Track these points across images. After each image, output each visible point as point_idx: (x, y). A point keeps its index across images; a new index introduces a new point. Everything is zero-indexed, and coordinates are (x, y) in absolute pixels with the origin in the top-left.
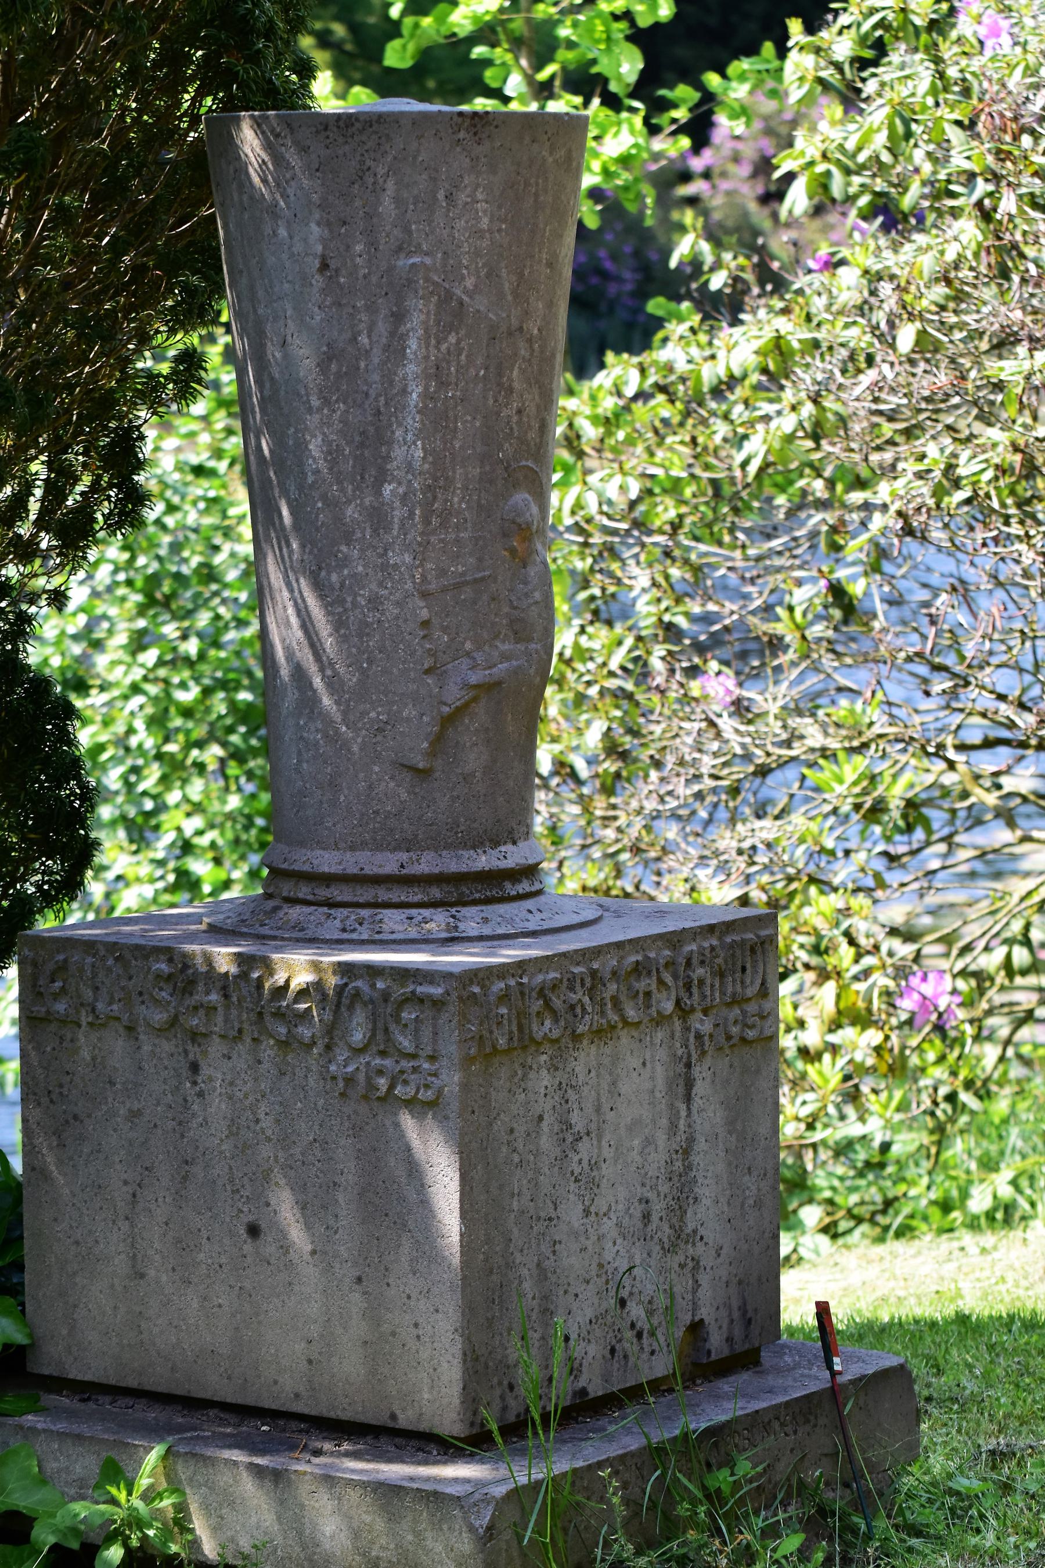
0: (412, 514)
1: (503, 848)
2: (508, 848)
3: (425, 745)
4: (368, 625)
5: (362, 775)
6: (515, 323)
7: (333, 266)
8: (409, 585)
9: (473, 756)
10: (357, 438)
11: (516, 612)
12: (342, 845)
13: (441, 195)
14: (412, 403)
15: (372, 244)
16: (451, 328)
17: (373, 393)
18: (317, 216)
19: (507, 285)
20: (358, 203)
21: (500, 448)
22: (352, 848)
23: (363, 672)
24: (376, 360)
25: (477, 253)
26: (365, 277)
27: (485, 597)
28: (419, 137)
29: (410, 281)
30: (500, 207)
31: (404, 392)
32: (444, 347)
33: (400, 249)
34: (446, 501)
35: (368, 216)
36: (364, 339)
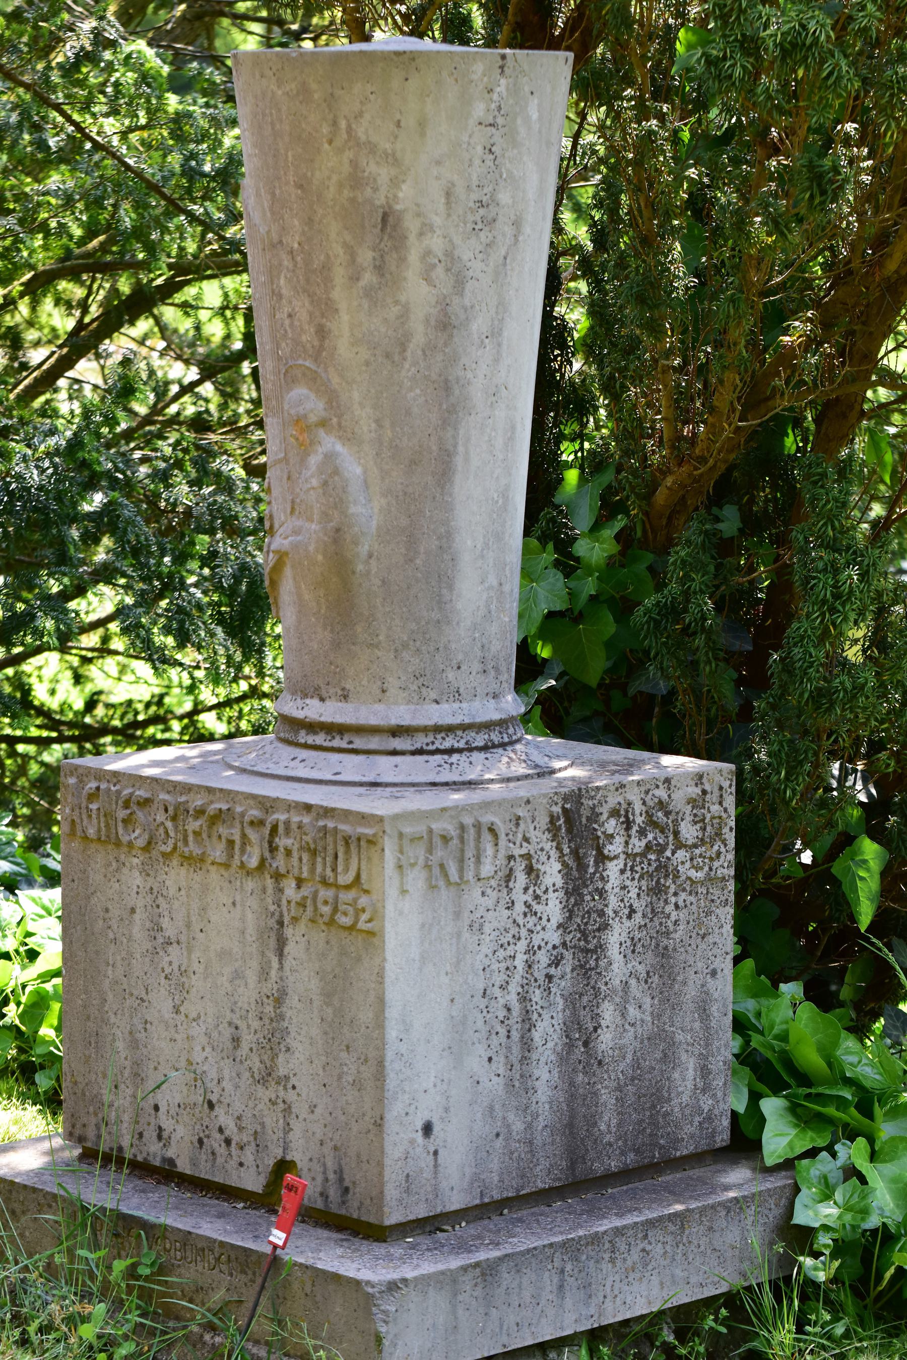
1: (308, 701)
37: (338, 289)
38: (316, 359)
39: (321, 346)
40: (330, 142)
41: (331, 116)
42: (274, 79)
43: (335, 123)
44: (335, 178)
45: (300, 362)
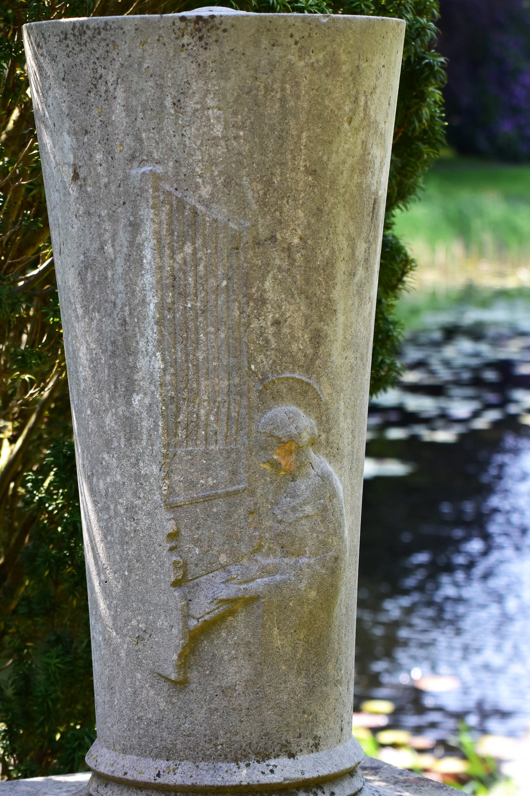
0: (156, 425)
1: (272, 762)
2: (283, 761)
3: (175, 657)
4: (127, 533)
5: (128, 681)
6: (263, 233)
7: (81, 176)
8: (157, 497)
9: (232, 670)
10: (110, 348)
11: (281, 527)
12: (118, 747)
13: (168, 102)
14: (151, 314)
15: (109, 153)
16: (183, 239)
17: (119, 302)
18: (67, 125)
19: (250, 194)
20: (95, 112)
21: (251, 359)
22: (124, 751)
23: (126, 579)
24: (120, 270)
25: (212, 162)
26: (106, 186)
27: (241, 511)
28: (143, 43)
29: (142, 189)
30: (235, 113)
31: (144, 302)
32: (179, 257)
33: (133, 157)
34: (191, 413)
35: (104, 125)
36: (109, 249)
37: (338, 287)
38: (308, 369)
40: (350, 123)
41: (353, 92)
42: (294, 49)
43: (356, 101)
44: (349, 161)
45: (287, 375)
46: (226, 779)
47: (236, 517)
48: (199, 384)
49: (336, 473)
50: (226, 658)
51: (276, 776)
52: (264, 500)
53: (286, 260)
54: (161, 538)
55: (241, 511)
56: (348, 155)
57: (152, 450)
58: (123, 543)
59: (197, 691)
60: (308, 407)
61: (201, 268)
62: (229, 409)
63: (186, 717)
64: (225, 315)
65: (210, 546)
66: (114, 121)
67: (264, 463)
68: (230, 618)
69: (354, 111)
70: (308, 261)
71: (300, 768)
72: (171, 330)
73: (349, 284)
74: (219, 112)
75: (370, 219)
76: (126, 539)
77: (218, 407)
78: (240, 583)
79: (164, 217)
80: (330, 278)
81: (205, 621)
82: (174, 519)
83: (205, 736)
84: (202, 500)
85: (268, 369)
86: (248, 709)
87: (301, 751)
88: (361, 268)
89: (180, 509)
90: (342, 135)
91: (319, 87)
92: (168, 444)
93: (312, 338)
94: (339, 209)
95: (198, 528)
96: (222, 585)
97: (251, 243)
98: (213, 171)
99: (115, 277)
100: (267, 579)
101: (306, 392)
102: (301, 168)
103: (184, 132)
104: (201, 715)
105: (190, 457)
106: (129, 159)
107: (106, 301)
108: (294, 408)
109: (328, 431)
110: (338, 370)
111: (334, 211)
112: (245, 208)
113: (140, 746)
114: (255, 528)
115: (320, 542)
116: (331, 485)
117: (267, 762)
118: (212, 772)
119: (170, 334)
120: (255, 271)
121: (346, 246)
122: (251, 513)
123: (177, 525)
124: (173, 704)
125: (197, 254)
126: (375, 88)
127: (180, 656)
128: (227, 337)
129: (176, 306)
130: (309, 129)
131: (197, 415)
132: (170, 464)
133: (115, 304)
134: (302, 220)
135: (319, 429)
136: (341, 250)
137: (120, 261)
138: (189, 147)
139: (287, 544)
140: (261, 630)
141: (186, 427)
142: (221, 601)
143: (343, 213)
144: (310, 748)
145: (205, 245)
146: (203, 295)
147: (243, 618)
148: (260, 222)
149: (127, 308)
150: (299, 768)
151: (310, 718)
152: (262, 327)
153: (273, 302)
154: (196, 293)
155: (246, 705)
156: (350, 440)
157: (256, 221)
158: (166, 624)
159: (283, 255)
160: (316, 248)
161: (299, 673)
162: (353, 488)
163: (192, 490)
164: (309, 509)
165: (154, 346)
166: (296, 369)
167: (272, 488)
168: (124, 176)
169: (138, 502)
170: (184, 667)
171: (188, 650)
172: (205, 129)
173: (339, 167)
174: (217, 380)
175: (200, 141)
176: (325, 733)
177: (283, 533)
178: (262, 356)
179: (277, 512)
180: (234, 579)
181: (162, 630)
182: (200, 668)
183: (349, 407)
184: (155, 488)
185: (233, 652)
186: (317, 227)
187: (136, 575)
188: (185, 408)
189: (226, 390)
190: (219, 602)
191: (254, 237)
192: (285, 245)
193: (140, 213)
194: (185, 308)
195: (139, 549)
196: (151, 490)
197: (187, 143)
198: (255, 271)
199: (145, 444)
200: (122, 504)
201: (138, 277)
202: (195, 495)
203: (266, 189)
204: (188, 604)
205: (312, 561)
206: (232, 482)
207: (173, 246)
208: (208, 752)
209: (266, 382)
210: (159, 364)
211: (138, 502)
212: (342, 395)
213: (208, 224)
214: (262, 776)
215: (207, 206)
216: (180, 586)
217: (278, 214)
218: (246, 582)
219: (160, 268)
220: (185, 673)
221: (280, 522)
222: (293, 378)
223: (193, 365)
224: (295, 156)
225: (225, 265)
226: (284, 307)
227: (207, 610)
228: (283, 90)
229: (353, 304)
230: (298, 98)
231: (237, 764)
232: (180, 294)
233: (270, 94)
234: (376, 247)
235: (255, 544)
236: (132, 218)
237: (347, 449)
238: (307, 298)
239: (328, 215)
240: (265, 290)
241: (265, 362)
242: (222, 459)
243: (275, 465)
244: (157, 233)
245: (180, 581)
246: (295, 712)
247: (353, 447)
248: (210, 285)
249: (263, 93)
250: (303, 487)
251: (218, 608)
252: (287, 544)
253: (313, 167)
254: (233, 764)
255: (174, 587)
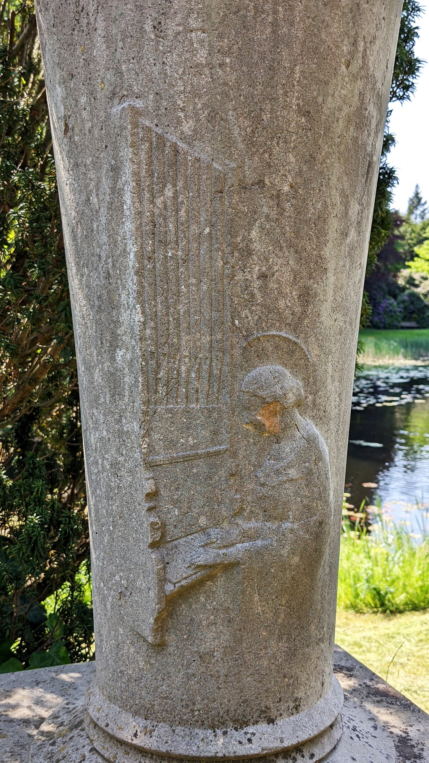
0: (137, 381)
1: (251, 729)
2: (263, 727)
3: (152, 620)
6: (251, 176)
8: (137, 455)
10: (97, 303)
11: (264, 490)
13: (148, 28)
14: (131, 264)
15: (92, 94)
17: (103, 255)
20: (78, 52)
24: (103, 220)
25: (196, 93)
27: (223, 473)
30: (221, 36)
32: (159, 201)
34: (171, 369)
36: (94, 200)
37: (330, 245)
38: (295, 328)
39: (304, 312)
40: (348, 66)
43: (355, 44)
44: (346, 110)
46: (201, 748)
47: (217, 478)
48: (179, 339)
49: (322, 436)
50: (204, 623)
51: (253, 747)
52: (247, 462)
53: (275, 209)
54: (140, 497)
55: (223, 473)
56: (344, 102)
57: (133, 406)
58: (110, 498)
59: (175, 655)
60: (295, 368)
61: (182, 213)
62: (211, 366)
63: (163, 680)
64: (208, 265)
65: (189, 508)
66: (95, 57)
67: (247, 423)
68: (209, 583)
69: (352, 54)
70: (299, 212)
71: (279, 735)
72: (151, 280)
73: (341, 244)
74: (203, 34)
75: (364, 181)
76: (111, 495)
77: (200, 364)
78: (220, 548)
79: (143, 156)
80: (322, 233)
81: (182, 586)
82: (153, 478)
83: (182, 700)
84: (181, 460)
85: (253, 326)
86: (226, 676)
87: (281, 715)
88: (353, 230)
89: (159, 468)
90: (339, 78)
91: (316, 17)
92: (149, 401)
93: (300, 295)
94: (333, 160)
95: (177, 489)
96: (201, 548)
97: (236, 187)
98: (196, 103)
99: (100, 228)
100: (247, 544)
101: (293, 352)
102: (294, 107)
103: (165, 60)
104: (178, 679)
105: (170, 415)
106: (109, 96)
107: (93, 255)
108: (280, 368)
109: (315, 393)
110: (327, 332)
111: (328, 161)
112: (231, 147)
113: (122, 699)
114: (236, 490)
115: (304, 506)
116: (317, 447)
117: (245, 730)
118: (188, 739)
119: (150, 285)
120: (240, 217)
121: (339, 202)
122: (232, 475)
123: (156, 484)
124: (151, 664)
125: (178, 197)
126: (375, 38)
127: (156, 620)
128: (210, 290)
129: (156, 255)
130: (303, 63)
131: (178, 371)
132: (150, 422)
133: (100, 256)
134: (293, 165)
135: (306, 391)
136: (334, 205)
137: (103, 211)
138: (171, 76)
139: (271, 509)
140: (241, 597)
141: (167, 384)
142: (198, 566)
143: (337, 165)
144: (290, 711)
145: (186, 187)
146: (184, 243)
147: (222, 583)
148: (247, 164)
149: (110, 260)
150: (278, 735)
151: (291, 681)
152: (247, 280)
153: (259, 254)
154: (177, 241)
155: (223, 672)
156: (337, 403)
157: (243, 162)
158: (144, 585)
159: (271, 203)
160: (308, 198)
161: (280, 638)
162: (338, 449)
163: (172, 449)
164: (293, 473)
165: (134, 298)
166: (283, 327)
167: (255, 449)
168: (105, 117)
169: (121, 459)
170: (161, 631)
171: (165, 614)
172: (188, 55)
173: (334, 114)
174: (198, 335)
175: (182, 69)
176: (306, 693)
177: (266, 496)
178: (247, 311)
179: (260, 474)
180: (214, 543)
181: (141, 591)
182: (178, 632)
183: (337, 370)
184: (136, 446)
185: (212, 617)
186: (308, 176)
187: (119, 531)
188: (165, 363)
189: (208, 346)
190: (195, 568)
191: (240, 180)
192: (274, 193)
193: (121, 154)
194: (166, 257)
195: (122, 506)
196: (132, 448)
197: (168, 72)
198: (240, 217)
199: (127, 400)
200: (108, 459)
201: (119, 226)
202: (175, 455)
203: (254, 126)
204: (165, 567)
205: (296, 526)
206: (213, 442)
207: (153, 188)
208: (185, 717)
209: (250, 339)
210: (139, 317)
211: (121, 459)
212: (330, 357)
213: (190, 164)
214: (239, 746)
215: (189, 144)
216: (158, 548)
217: (267, 155)
218: (225, 547)
219: (140, 213)
220: (162, 636)
221: (263, 485)
222: (279, 336)
223: (174, 319)
224: (287, 92)
225: (208, 210)
226: (271, 260)
227: (185, 575)
228: (275, 12)
229: (344, 266)
230: (292, 24)
231: (214, 732)
232: (160, 241)
233: (260, 16)
234: (369, 213)
235: (236, 508)
236: (113, 162)
237: (334, 412)
238: (296, 252)
239: (321, 164)
240: (251, 239)
241: (250, 318)
242: (203, 419)
243: (259, 427)
244: (136, 174)
245: (158, 542)
246: (275, 677)
247: (340, 410)
248: (191, 233)
249: (252, 14)
250: (288, 450)
251: (196, 573)
252: (271, 509)
253: (307, 108)
254: (210, 731)
255: (152, 548)
